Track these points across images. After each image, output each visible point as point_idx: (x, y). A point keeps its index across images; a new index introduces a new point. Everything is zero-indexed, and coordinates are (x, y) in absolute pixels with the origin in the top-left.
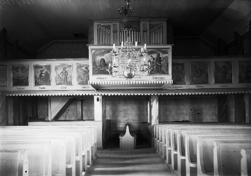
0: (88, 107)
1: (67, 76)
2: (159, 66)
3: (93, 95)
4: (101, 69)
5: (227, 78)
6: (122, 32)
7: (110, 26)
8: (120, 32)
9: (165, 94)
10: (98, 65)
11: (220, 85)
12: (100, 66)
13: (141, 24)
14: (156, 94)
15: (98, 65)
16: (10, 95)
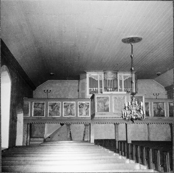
6: (105, 80)
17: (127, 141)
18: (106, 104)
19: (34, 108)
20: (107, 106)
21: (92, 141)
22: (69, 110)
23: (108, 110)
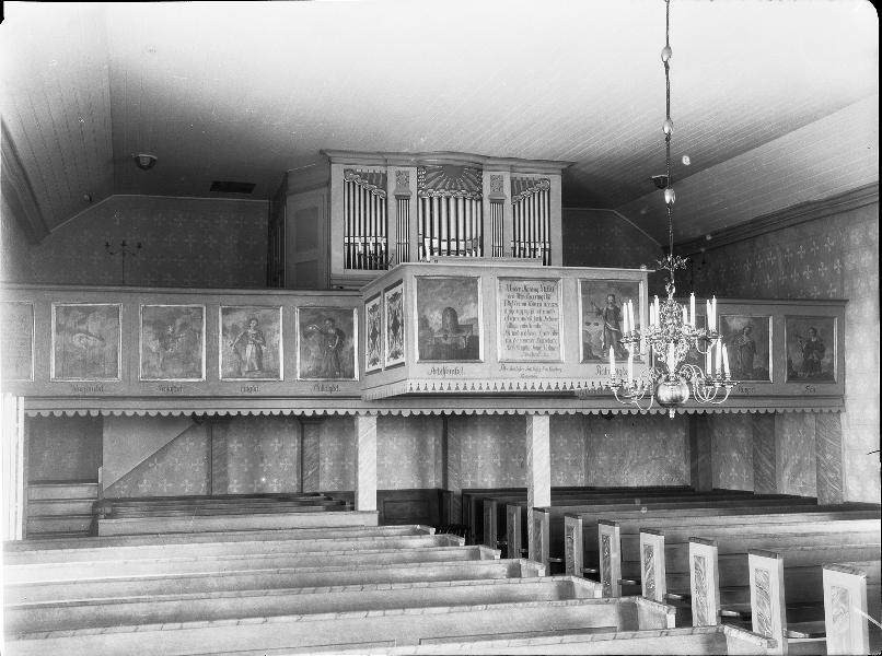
0: (262, 458)
1: (263, 347)
2: (613, 334)
3: (352, 412)
4: (444, 341)
5: (755, 367)
6: (424, 200)
7: (385, 177)
8: (418, 196)
9: (579, 411)
10: (436, 329)
11: (431, 365)
12: (443, 330)
13: (486, 177)
14: (406, 413)
15: (436, 329)
16: (79, 411)
17: (522, 494)
18: (461, 320)
19: (57, 331)
20: (471, 325)
21: (367, 500)
22: (250, 350)
23: (469, 352)
